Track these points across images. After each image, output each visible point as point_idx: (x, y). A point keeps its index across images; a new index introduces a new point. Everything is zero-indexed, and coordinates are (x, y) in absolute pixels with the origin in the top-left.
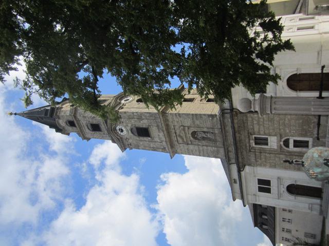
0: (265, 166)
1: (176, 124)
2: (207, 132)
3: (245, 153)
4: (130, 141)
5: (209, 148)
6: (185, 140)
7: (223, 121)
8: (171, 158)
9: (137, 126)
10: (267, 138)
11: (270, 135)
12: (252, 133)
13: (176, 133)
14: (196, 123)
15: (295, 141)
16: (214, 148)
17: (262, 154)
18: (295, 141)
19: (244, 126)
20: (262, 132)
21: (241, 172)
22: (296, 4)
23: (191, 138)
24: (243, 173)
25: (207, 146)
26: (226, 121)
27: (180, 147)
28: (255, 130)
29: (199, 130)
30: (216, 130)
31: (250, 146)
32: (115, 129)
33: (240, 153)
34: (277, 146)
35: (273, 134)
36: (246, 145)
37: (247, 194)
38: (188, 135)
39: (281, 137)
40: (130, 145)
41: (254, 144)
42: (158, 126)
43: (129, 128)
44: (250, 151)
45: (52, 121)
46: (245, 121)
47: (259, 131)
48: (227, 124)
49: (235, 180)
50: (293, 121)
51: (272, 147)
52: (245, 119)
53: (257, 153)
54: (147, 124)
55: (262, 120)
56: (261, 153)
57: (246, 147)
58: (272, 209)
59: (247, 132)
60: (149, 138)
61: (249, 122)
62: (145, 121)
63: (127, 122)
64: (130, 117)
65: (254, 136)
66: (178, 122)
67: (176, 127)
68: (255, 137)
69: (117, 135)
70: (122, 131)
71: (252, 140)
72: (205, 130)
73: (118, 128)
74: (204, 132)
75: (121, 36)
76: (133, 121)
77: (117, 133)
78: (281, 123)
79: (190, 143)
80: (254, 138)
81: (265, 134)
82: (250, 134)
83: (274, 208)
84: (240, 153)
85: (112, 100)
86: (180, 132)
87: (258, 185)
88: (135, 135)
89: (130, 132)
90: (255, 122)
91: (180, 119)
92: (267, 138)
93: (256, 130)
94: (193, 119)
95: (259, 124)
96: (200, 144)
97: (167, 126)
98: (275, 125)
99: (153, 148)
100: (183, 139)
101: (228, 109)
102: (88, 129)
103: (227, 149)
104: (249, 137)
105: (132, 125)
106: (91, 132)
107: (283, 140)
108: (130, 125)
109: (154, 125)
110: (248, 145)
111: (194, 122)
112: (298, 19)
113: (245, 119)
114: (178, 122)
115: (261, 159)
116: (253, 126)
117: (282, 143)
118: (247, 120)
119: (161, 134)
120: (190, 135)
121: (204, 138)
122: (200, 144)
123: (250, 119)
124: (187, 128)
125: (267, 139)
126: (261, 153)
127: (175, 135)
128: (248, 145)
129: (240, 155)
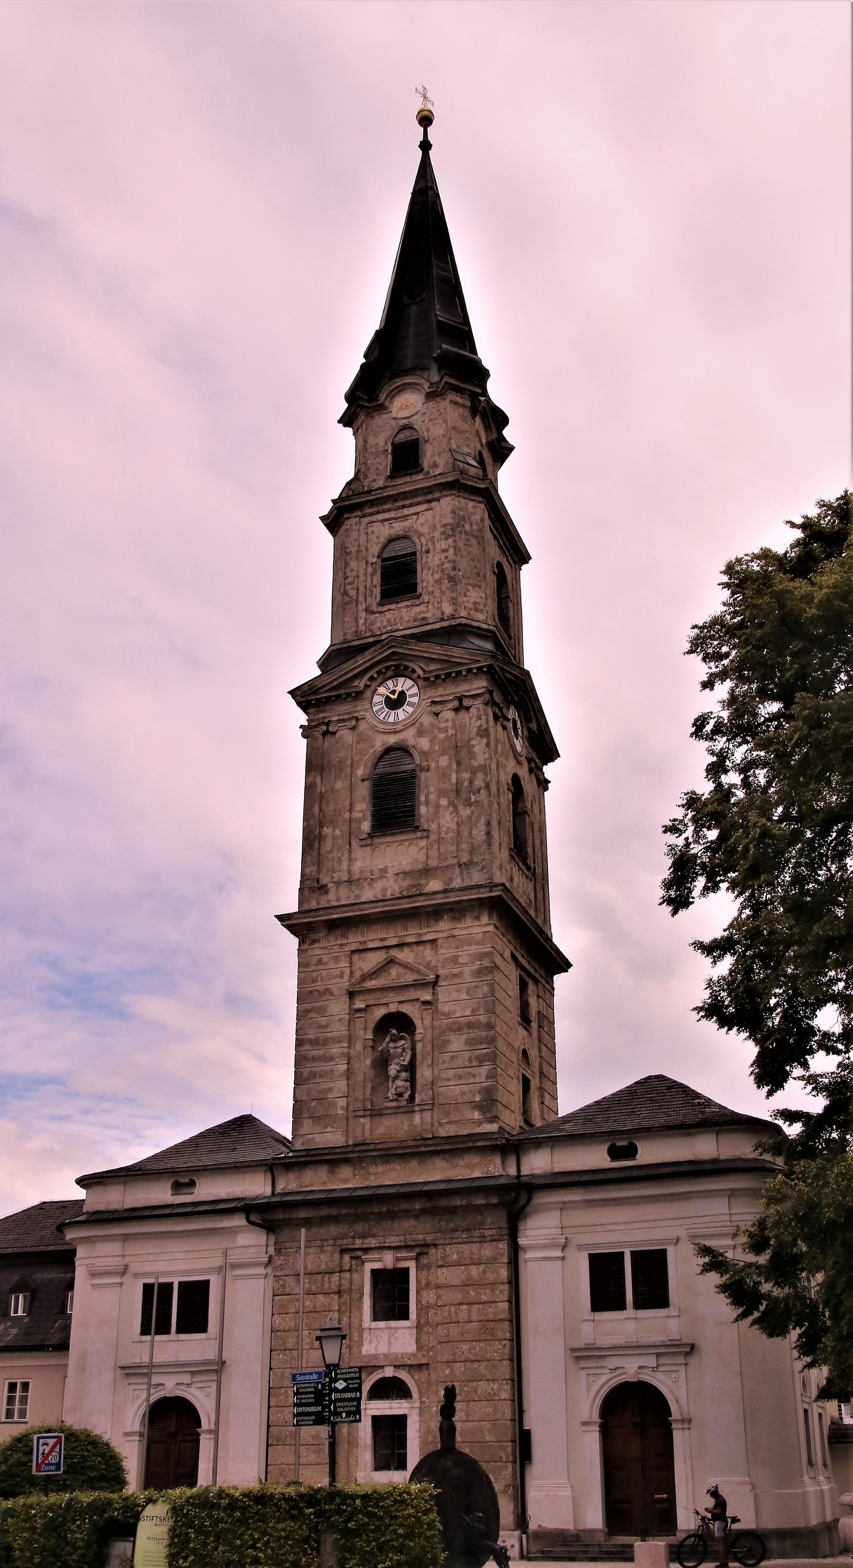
0: (279, 1309)
1: (446, 952)
2: (412, 1081)
3: (334, 1230)
4: (345, 735)
5: (341, 1085)
6: (371, 984)
7: (468, 1150)
8: (281, 918)
9: (423, 776)
10: (406, 1317)
11: (419, 1327)
12: (424, 1261)
13: (400, 946)
14: (452, 1037)
15: (401, 1420)
16: (342, 1102)
17: (336, 1297)
18: (401, 1420)
19: (454, 1230)
20: (430, 1297)
21: (244, 1216)
22: (741, 1392)
23: (380, 1012)
24: (239, 1221)
25: (349, 1074)
26: (474, 1159)
27: (336, 959)
28: (440, 1271)
29: (419, 1046)
30: (427, 1116)
31: (366, 1250)
32: (400, 672)
33: (334, 1212)
34: (375, 1356)
35: (424, 1337)
36: (374, 1236)
37: (126, 1238)
38: (393, 997)
39: (412, 1368)
40: (325, 734)
41: (377, 1266)
42: (426, 872)
43: (408, 736)
44: (343, 1251)
45: (409, 353)
46: (476, 1233)
47: (438, 1287)
48: (461, 1162)
49: (192, 1184)
50: (490, 1410)
51: (366, 1336)
52: (486, 1233)
53: (335, 1278)
54: (434, 826)
55: (484, 1298)
56: (339, 1292)
57: (363, 1236)
58: (55, 1340)
59: (429, 1238)
60: (366, 826)
61: (475, 1247)
62: (448, 820)
63: (442, 736)
64: (463, 754)
65: (412, 1265)
66: (454, 960)
67: (427, 952)
68: (406, 1270)
69: (372, 679)
70: (395, 703)
71: (398, 1260)
72: (424, 1073)
73: (403, 684)
74: (411, 1067)
75: (694, 816)
76: (444, 761)
77: (383, 677)
78: (475, 1365)
79: (359, 1004)
80: (403, 1264)
81: (422, 1309)
82: (421, 1250)
83: (63, 1346)
84: (334, 1212)
85: (470, 724)
86: (406, 966)
87: (630, 1311)
88: (375, 766)
89: (392, 740)
90: (474, 1271)
91: (467, 971)
92: (406, 1317)
93: (443, 1275)
94: (470, 1025)
95: (467, 1284)
96: (359, 1046)
97: (436, 913)
98: (465, 1347)
99: (321, 838)
100: (374, 974)
101: (519, 1170)
102: (391, 541)
103: (347, 1161)
104: (407, 1247)
105: (425, 754)
106: (375, 549)
107: (403, 1375)
108: (424, 743)
109: (434, 853)
110: (373, 1242)
111: (458, 1028)
112: (806, 1408)
113: (486, 1233)
114: (454, 960)
115: (309, 1293)
116: (457, 1264)
117: (389, 1372)
118: (483, 1240)
119: (392, 886)
120: (393, 1008)
121: (382, 1063)
122: (359, 1046)
123: (488, 1250)
124: (428, 997)
125: (404, 1315)
126: (339, 1292)
127: (394, 942)
128: (373, 1242)
129: (324, 1212)
